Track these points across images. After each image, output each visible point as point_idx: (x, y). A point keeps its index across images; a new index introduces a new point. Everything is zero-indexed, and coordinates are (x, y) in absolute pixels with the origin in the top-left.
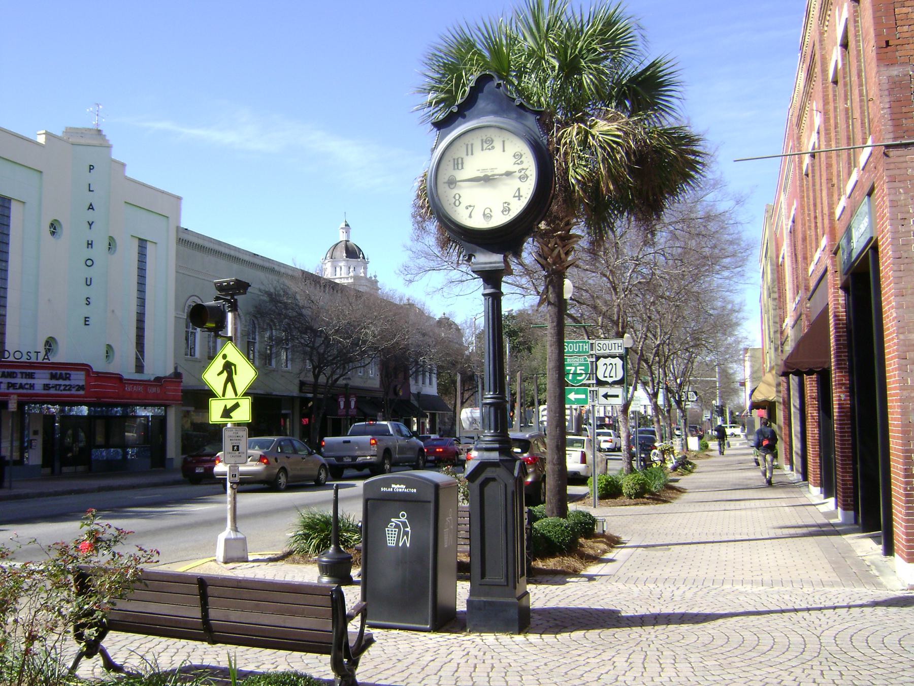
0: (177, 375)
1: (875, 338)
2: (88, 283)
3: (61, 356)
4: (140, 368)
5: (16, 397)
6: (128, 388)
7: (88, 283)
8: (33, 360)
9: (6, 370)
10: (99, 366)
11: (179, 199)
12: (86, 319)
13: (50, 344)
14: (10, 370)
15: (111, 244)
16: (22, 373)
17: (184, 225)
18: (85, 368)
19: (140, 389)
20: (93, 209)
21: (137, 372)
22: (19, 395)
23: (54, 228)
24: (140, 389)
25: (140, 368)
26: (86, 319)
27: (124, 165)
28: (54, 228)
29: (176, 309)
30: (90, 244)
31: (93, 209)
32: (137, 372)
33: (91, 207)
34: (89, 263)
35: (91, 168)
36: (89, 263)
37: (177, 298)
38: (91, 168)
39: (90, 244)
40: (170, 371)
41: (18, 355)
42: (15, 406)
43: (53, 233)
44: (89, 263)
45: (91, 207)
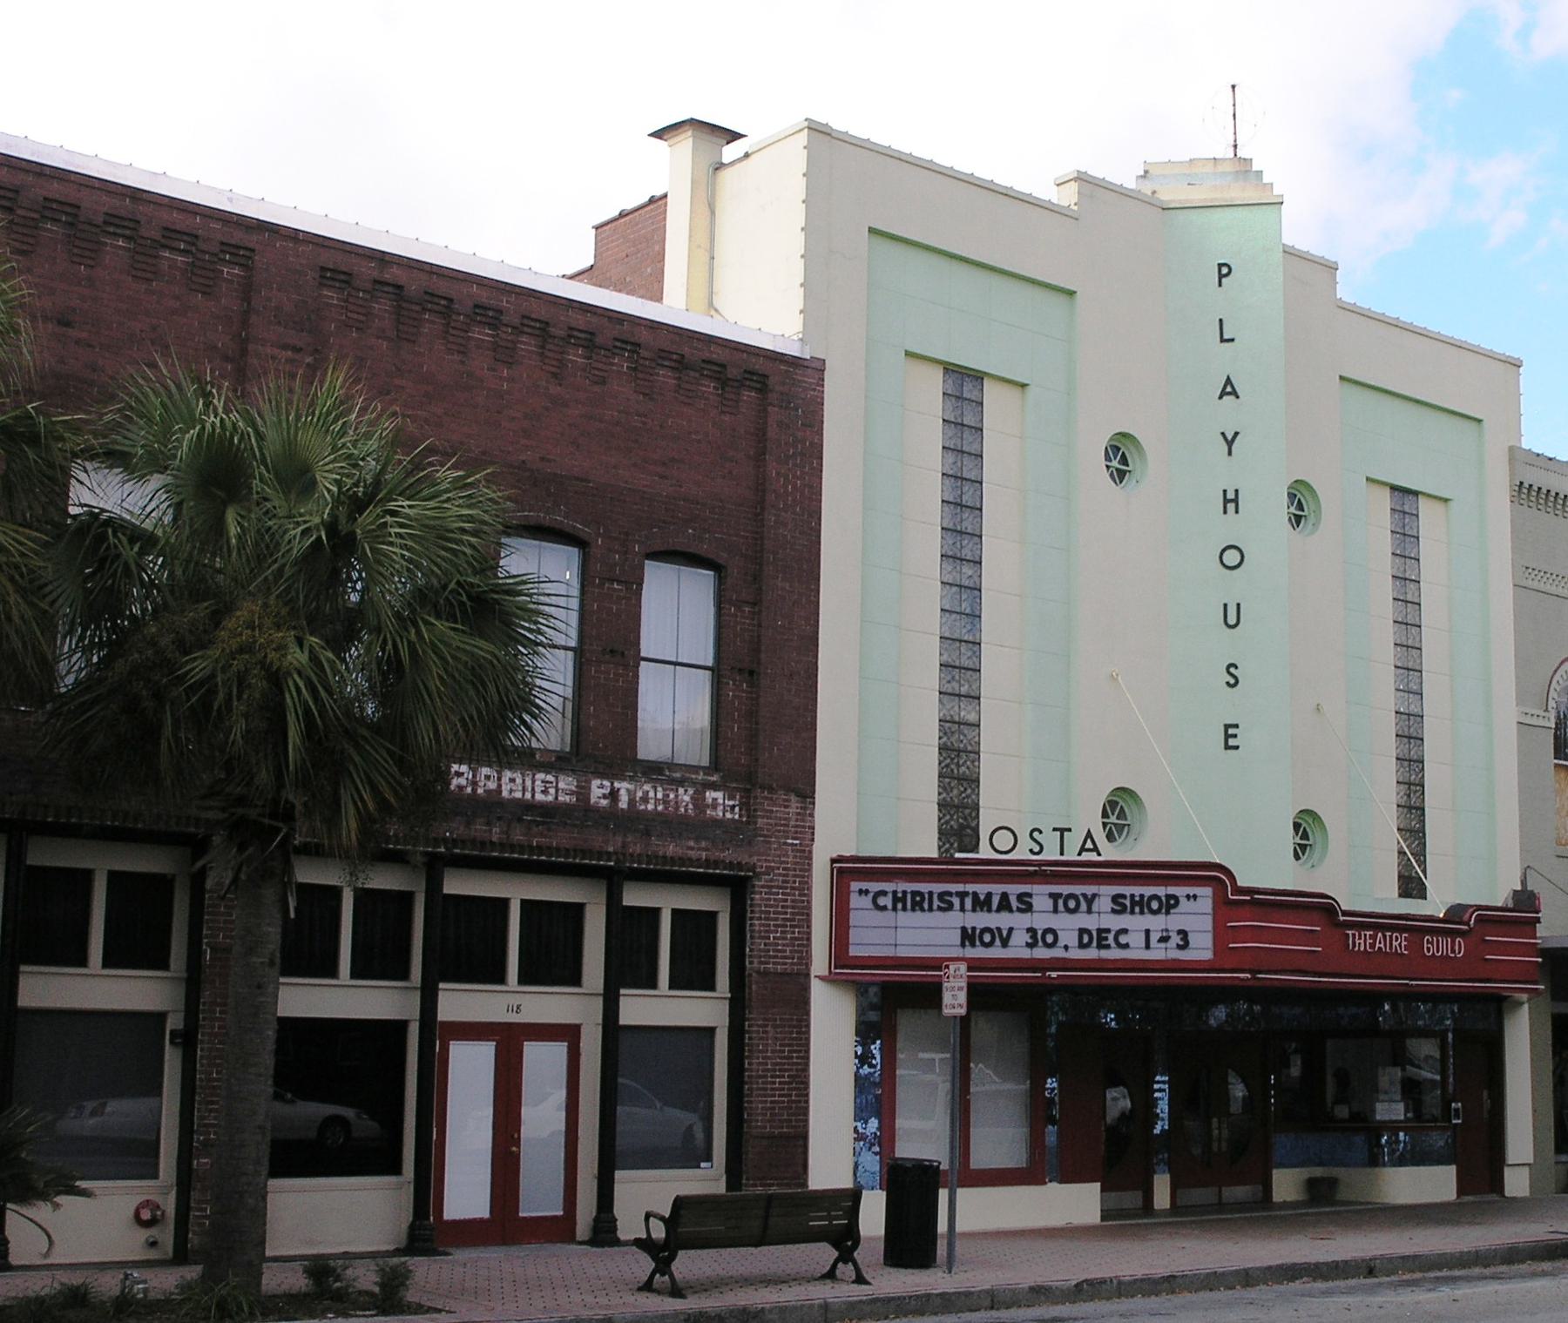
0: (1526, 900)
1: (306, 981)
2: (1232, 619)
3: (1152, 843)
4: (1411, 886)
5: (963, 967)
6: (1361, 942)
7: (1232, 619)
8: (1051, 854)
9: (1127, 890)
10: (1266, 866)
11: (1517, 365)
12: (1229, 731)
13: (1119, 809)
14: (1137, 890)
15: (1300, 505)
16: (962, 895)
17: (1535, 439)
18: (1213, 875)
19: (1399, 942)
20: (1234, 393)
21: (1405, 892)
22: (973, 964)
23: (1121, 457)
24: (1399, 942)
25: (1411, 886)
26: (1229, 731)
27: (1332, 268)
28: (1121, 457)
29: (1520, 700)
30: (1231, 501)
31: (1228, 381)
32: (1405, 892)
33: (1229, 389)
34: (1232, 557)
35: (1224, 271)
36: (1232, 558)
37: (1523, 662)
38: (1224, 271)
39: (1231, 501)
40: (1498, 895)
41: (1003, 841)
42: (962, 997)
43: (1120, 476)
44: (1232, 557)
45: (1229, 389)
